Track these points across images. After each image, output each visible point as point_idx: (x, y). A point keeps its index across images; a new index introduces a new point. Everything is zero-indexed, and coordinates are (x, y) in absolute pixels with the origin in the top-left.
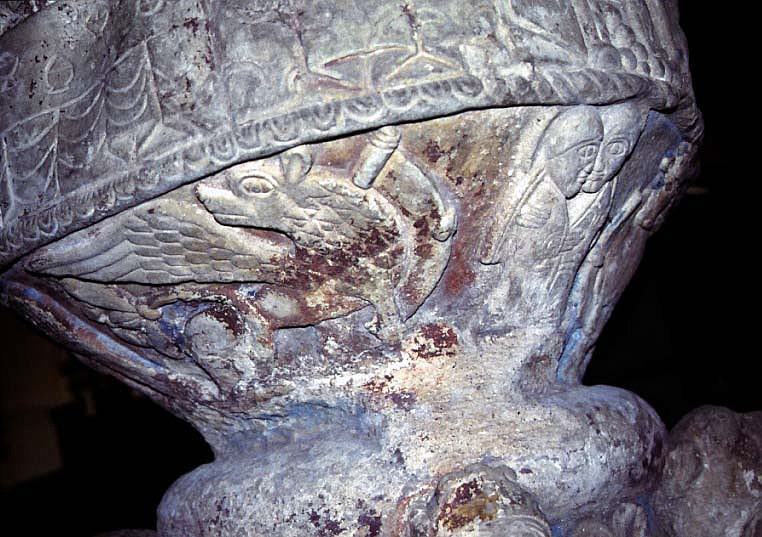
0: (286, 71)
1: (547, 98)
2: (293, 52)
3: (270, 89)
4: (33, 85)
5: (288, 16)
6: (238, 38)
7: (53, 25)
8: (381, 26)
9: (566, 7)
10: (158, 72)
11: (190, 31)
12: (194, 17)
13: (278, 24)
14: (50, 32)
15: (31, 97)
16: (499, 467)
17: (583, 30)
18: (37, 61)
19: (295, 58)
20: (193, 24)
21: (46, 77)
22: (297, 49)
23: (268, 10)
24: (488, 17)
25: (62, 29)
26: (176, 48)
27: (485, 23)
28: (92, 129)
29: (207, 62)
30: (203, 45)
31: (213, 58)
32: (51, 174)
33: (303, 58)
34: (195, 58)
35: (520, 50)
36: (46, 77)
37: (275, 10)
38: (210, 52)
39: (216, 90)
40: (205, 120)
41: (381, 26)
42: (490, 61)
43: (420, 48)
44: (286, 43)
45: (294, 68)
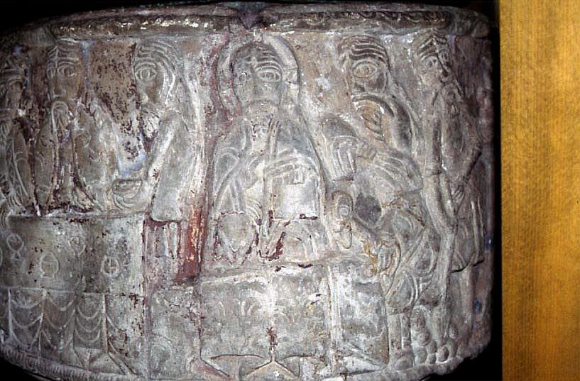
0: (186, 355)
1: (299, 47)
2: (192, 343)
3: (175, 363)
4: (31, 266)
5: (195, 316)
6: (161, 322)
7: (49, 232)
8: (251, 340)
9: (381, 330)
10: (109, 320)
11: (133, 302)
12: (136, 293)
13: (187, 320)
14: (45, 236)
15: (29, 273)
16: (191, 243)
17: (390, 344)
18: (36, 251)
19: (193, 348)
20: (134, 297)
21: (40, 264)
22: (196, 341)
23: (183, 306)
24: (324, 343)
25: (55, 237)
26: (122, 310)
27: (320, 348)
28: (65, 326)
29: (140, 329)
30: (139, 315)
31: (143, 326)
32: (37, 336)
33: (198, 348)
34: (133, 323)
35: (340, 366)
36: (40, 264)
37: (188, 308)
38: (143, 322)
39: (142, 350)
40: (133, 367)
41: (251, 340)
42: (317, 373)
43: (273, 359)
44: (190, 336)
45: (192, 354)
